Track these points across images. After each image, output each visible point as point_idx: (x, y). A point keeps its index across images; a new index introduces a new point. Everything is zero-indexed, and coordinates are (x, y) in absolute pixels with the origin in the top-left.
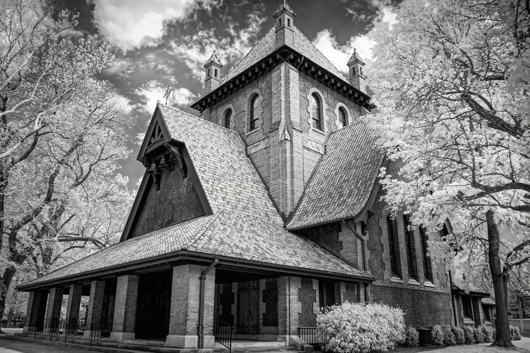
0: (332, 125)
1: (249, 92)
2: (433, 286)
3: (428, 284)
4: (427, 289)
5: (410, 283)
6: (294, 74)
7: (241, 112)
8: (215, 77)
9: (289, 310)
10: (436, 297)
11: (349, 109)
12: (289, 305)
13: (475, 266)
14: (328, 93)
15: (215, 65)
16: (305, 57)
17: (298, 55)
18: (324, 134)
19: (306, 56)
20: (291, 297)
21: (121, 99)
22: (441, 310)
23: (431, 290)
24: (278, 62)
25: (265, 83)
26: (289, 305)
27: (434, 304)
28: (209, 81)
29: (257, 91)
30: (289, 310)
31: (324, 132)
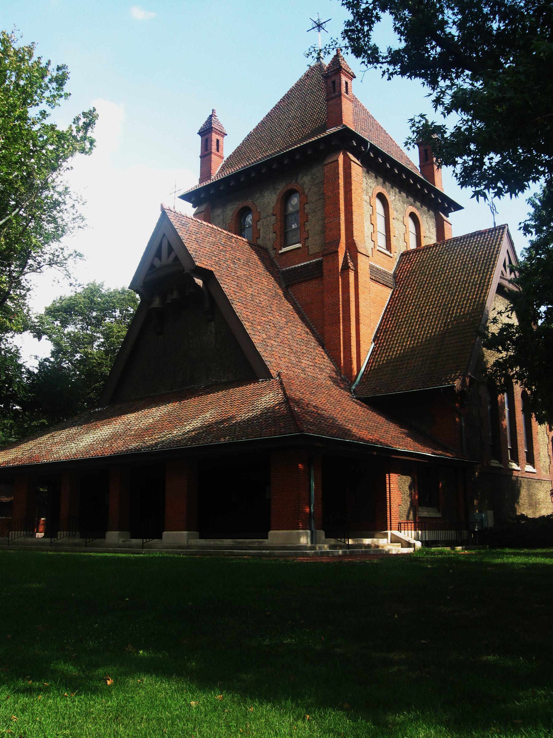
0: (401, 242)
1: (281, 188)
2: (534, 471)
3: (529, 468)
4: (528, 475)
5: (493, 465)
6: (357, 170)
7: (268, 216)
8: (217, 153)
9: (390, 502)
10: (537, 485)
11: (421, 214)
12: (390, 496)
13: (77, 200)
14: (395, 193)
15: (216, 133)
16: (371, 144)
17: (362, 142)
18: (391, 255)
19: (373, 143)
20: (392, 486)
21: (195, 246)
22: (542, 502)
23: (531, 475)
24: (336, 150)
25: (309, 177)
26: (390, 496)
27: (535, 494)
28: (208, 157)
29: (293, 186)
30: (390, 502)
31: (391, 253)
